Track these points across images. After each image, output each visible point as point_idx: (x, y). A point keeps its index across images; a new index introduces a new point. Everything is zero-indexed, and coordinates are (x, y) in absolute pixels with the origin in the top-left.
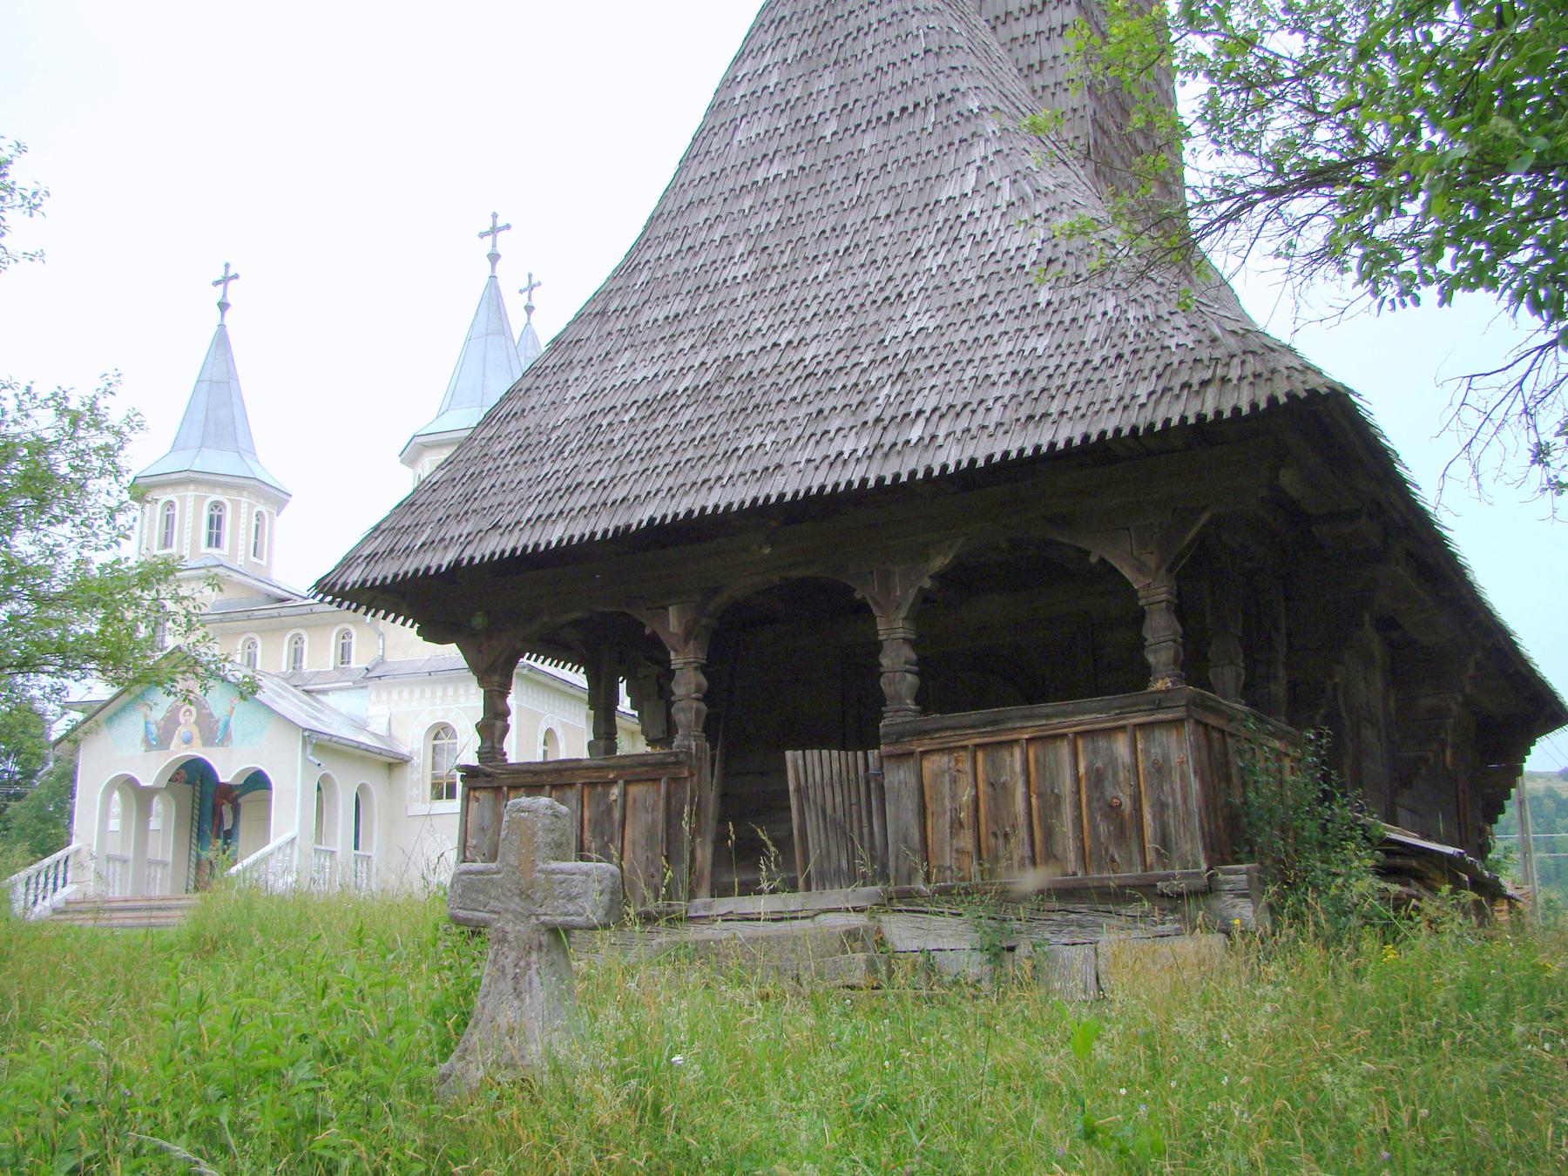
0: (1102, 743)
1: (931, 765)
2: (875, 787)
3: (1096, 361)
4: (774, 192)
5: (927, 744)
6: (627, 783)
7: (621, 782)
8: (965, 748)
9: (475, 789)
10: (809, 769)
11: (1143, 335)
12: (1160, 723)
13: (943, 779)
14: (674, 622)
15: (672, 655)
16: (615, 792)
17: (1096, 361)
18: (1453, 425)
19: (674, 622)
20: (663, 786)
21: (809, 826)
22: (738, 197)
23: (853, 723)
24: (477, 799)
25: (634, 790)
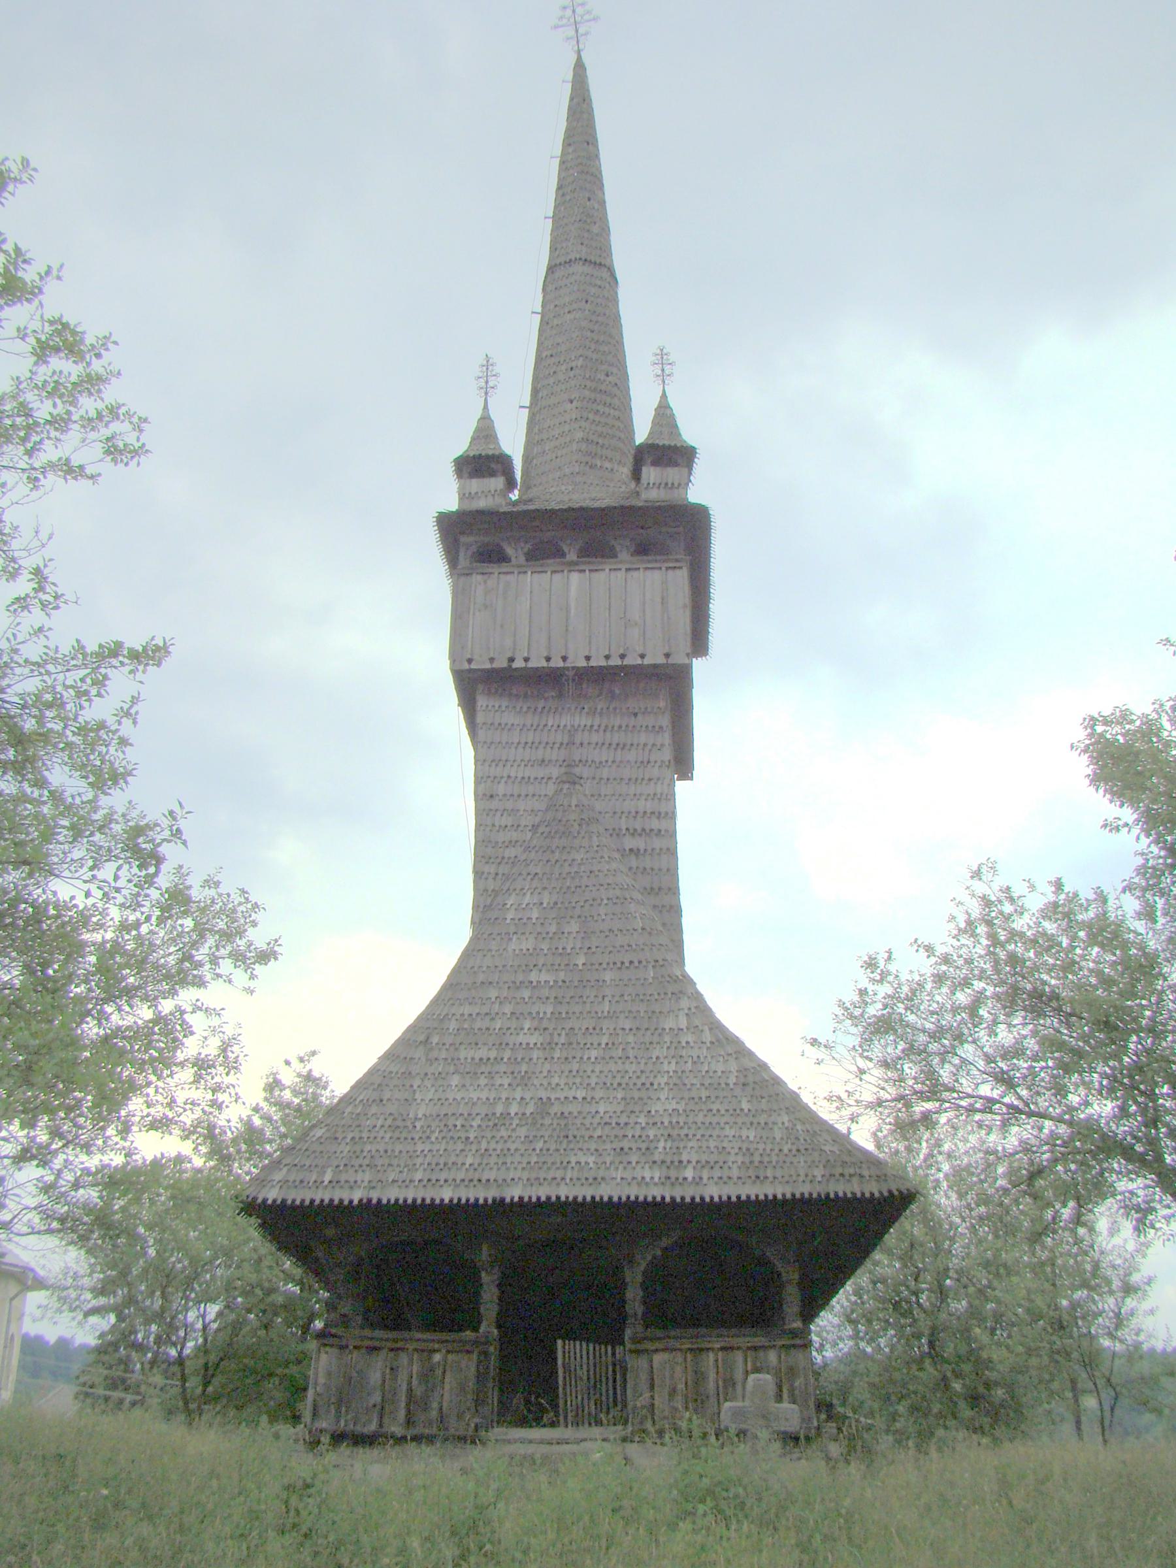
0: (761, 1354)
1: (658, 1358)
2: (620, 1369)
3: (786, 1151)
4: (545, 992)
5: (657, 1345)
6: (448, 1352)
7: (444, 1351)
8: (680, 1350)
9: (325, 1345)
10: (573, 1356)
11: (666, 1124)
12: (794, 1346)
13: (661, 1369)
14: (485, 1253)
15: (483, 1274)
16: (437, 1357)
17: (786, 1151)
18: (425, 1354)
19: (485, 1253)
20: (475, 1356)
21: (571, 1393)
22: (518, 988)
23: (606, 1327)
24: (327, 1353)
25: (450, 1357)
